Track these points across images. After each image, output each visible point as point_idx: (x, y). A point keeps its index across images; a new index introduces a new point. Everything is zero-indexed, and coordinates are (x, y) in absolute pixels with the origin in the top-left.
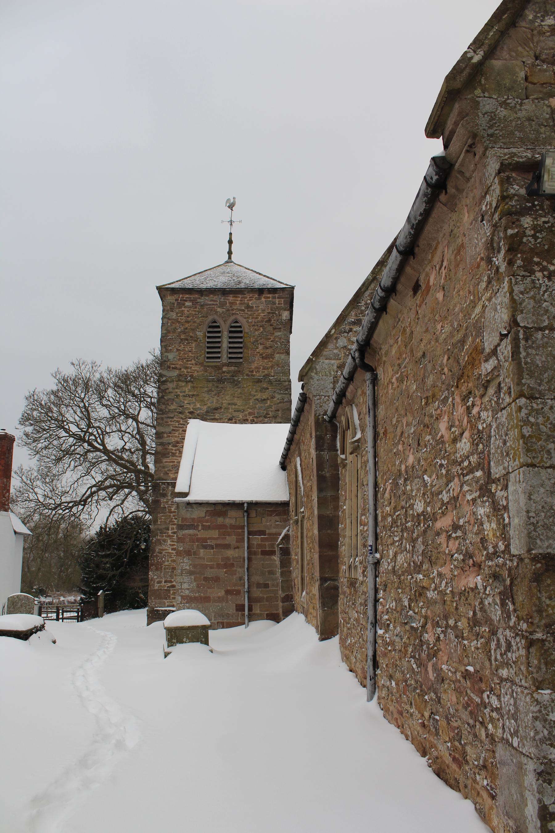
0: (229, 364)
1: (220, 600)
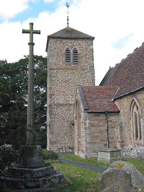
1: (99, 143)
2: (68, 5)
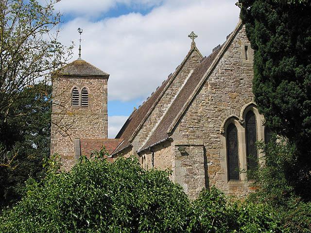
2: (81, 31)
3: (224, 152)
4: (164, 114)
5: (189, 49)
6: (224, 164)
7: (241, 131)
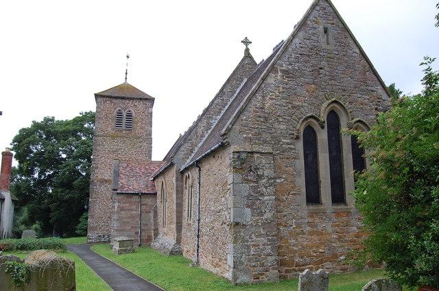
0: (125, 130)
3: (300, 164)
4: (213, 127)
5: (242, 55)
6: (301, 181)
7: (323, 136)
